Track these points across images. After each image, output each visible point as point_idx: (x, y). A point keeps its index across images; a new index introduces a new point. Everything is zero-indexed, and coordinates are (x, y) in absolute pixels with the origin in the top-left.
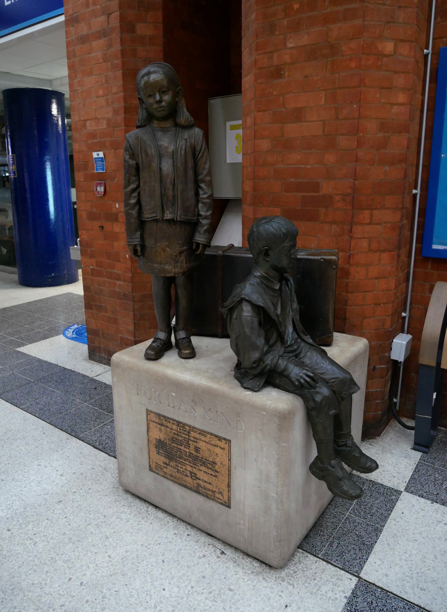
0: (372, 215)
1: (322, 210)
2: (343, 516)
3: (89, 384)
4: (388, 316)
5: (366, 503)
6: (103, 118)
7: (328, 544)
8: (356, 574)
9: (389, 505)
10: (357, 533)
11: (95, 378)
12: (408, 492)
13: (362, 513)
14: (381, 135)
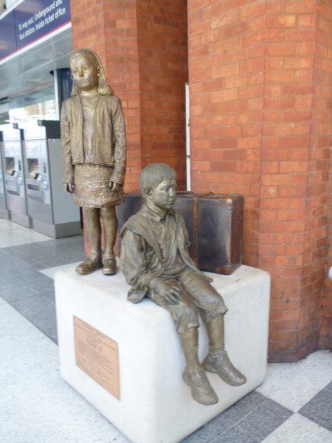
0: (279, 166)
1: (238, 163)
4: (300, 254)
14: (286, 96)
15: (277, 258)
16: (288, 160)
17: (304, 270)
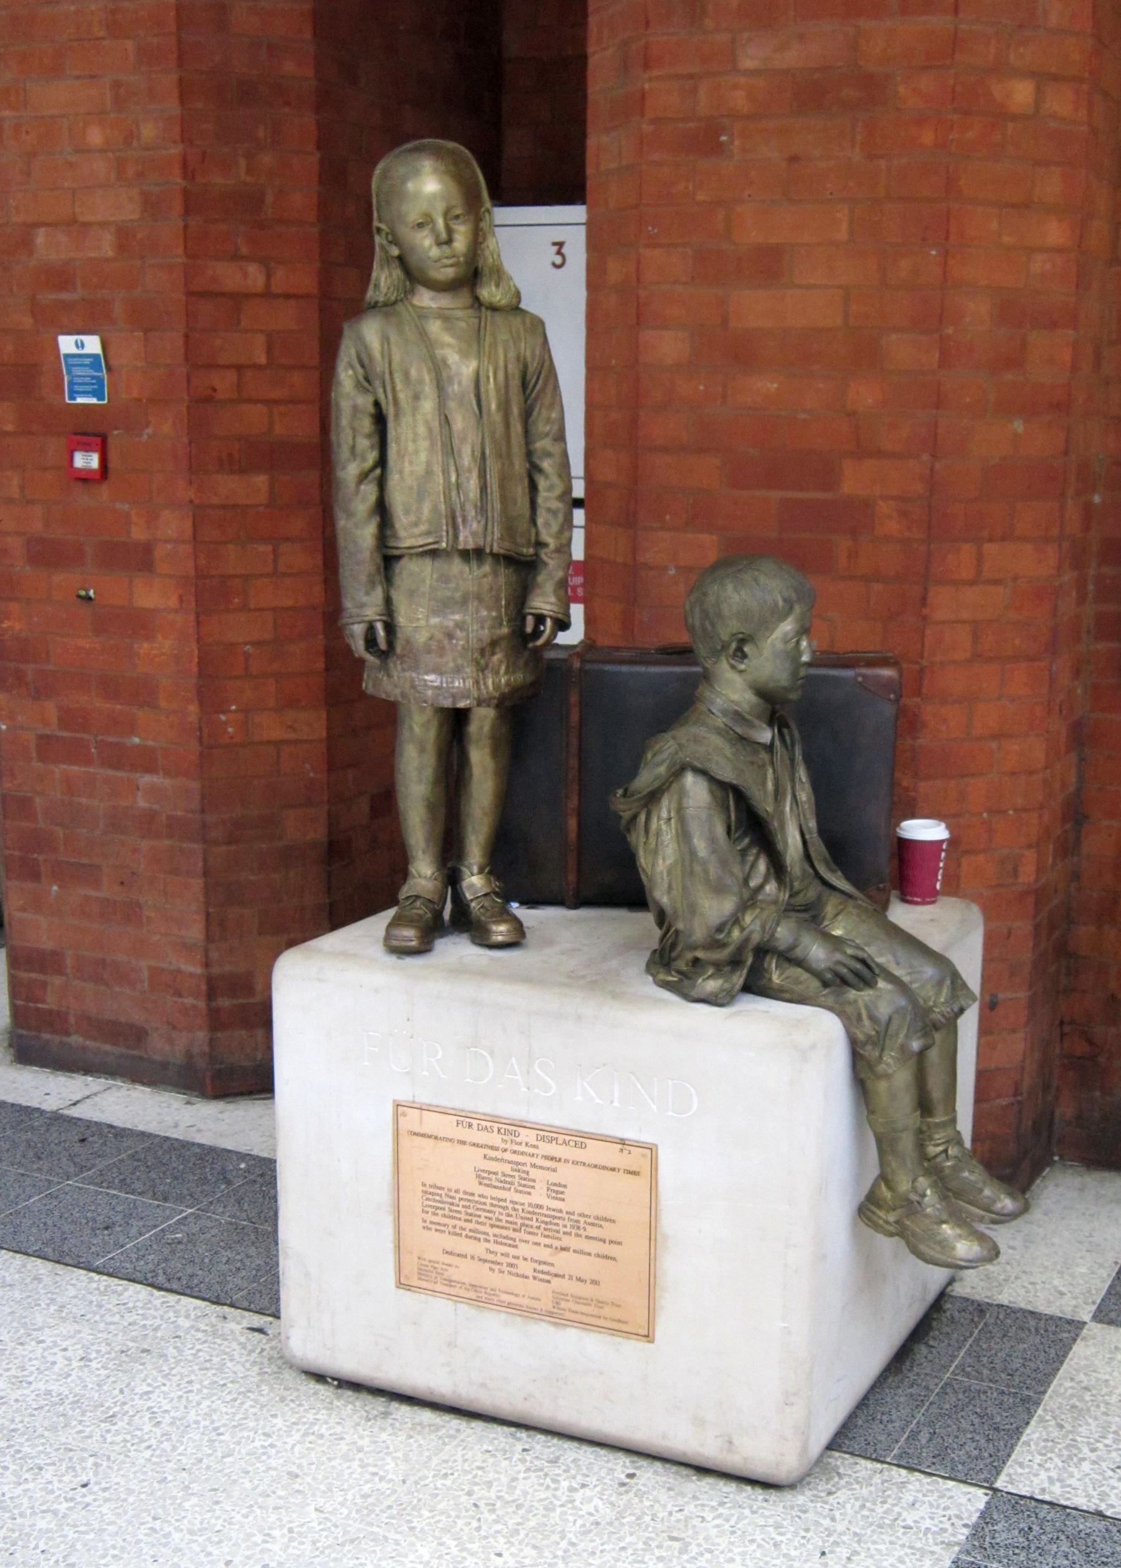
0: (980, 558)
1: (843, 544)
2: (936, 1380)
3: (53, 1129)
4: (1030, 846)
5: (993, 1352)
6: (103, 225)
7: (906, 1436)
8: (986, 1485)
9: (1053, 1351)
10: (978, 1410)
11: (66, 1112)
12: (1101, 1321)
13: (986, 1372)
15: (964, 861)
16: (1003, 539)
17: (1040, 895)
